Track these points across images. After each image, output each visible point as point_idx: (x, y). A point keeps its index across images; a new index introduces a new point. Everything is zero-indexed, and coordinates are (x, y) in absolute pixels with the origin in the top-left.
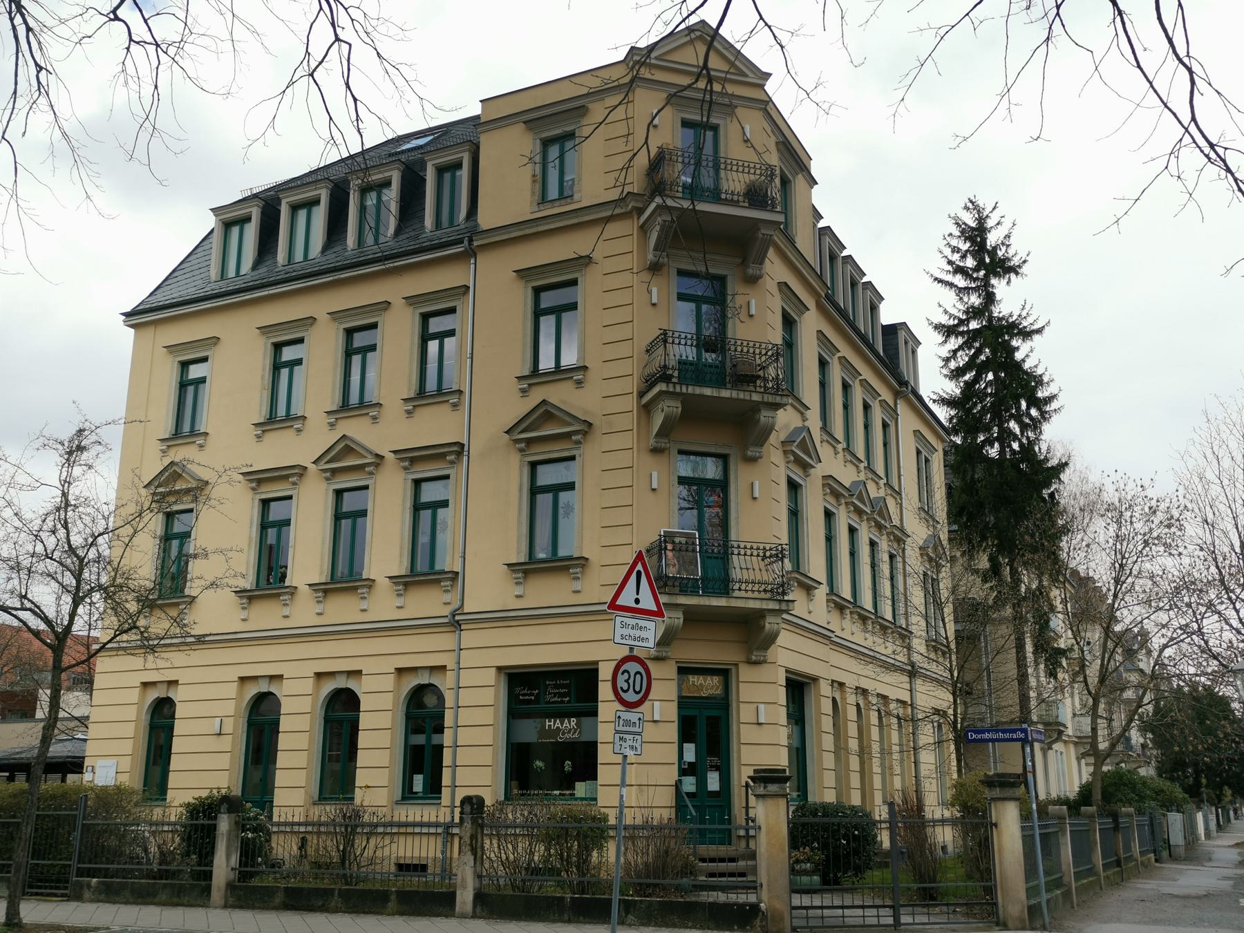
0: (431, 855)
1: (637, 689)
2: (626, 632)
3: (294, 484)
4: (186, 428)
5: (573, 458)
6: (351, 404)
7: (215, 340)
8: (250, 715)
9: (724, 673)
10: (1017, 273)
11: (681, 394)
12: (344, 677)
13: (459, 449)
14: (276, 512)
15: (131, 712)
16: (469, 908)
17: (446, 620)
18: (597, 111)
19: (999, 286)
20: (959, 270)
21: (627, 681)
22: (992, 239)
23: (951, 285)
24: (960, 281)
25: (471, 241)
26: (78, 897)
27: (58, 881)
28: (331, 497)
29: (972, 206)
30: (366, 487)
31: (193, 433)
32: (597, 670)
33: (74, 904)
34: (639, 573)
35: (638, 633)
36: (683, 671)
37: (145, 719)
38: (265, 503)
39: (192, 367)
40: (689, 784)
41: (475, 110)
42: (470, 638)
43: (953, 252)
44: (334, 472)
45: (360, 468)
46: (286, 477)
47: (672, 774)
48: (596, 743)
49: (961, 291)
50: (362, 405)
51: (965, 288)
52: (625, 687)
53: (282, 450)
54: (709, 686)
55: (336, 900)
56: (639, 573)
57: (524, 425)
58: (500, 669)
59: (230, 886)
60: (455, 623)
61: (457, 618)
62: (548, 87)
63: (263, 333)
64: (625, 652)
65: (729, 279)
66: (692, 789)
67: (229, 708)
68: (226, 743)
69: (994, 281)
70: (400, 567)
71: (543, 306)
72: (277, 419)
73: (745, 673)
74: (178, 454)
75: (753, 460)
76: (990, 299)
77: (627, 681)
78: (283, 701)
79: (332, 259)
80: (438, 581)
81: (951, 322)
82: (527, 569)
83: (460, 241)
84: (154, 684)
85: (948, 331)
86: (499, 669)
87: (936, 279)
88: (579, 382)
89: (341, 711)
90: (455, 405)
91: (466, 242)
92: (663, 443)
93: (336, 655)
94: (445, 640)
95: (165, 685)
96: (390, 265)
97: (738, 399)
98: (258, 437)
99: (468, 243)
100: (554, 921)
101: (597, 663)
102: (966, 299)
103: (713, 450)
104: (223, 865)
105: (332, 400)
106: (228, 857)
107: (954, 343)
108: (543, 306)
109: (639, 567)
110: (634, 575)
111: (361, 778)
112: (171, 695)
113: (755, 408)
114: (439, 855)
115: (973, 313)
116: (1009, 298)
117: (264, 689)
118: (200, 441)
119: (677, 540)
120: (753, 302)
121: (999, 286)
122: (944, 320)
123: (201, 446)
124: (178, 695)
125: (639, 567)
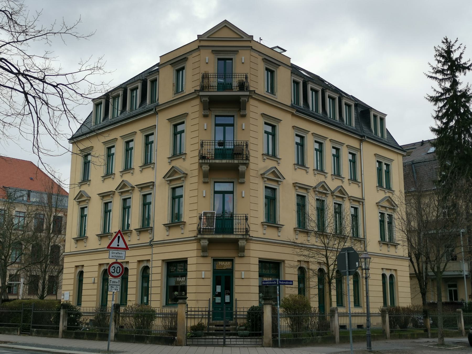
0: (159, 324)
1: (118, 272)
2: (113, 255)
6: (128, 168)
7: (186, 115)
8: (143, 274)
9: (232, 260)
10: (469, 69)
11: (207, 163)
12: (146, 262)
13: (153, 184)
14: (178, 192)
16: (113, 338)
17: (148, 244)
18: (190, 57)
19: (460, 76)
20: (442, 72)
21: (114, 270)
22: (455, 56)
23: (436, 78)
24: (440, 76)
25: (156, 109)
26: (31, 335)
27: (28, 330)
28: (170, 191)
29: (446, 41)
30: (182, 186)
31: (181, 154)
32: (187, 261)
33: (30, 337)
34: (119, 237)
35: (118, 255)
36: (215, 260)
38: (174, 189)
40: (218, 300)
41: (158, 61)
42: (156, 250)
43: (438, 62)
44: (171, 181)
45: (179, 179)
46: (109, 195)
47: (210, 296)
48: (187, 286)
49: (441, 80)
51: (443, 79)
52: (113, 271)
54: (227, 265)
55: (85, 336)
56: (119, 237)
58: (163, 261)
59: (63, 331)
60: (151, 245)
62: (182, 49)
63: (170, 121)
64: (115, 261)
65: (235, 116)
66: (219, 301)
67: (96, 274)
68: (95, 286)
69: (457, 74)
70: (167, 220)
72: (109, 174)
73: (237, 261)
74: (175, 163)
75: (243, 183)
76: (455, 83)
77: (114, 270)
79: (123, 116)
81: (438, 95)
83: (152, 110)
84: (142, 261)
85: (436, 100)
86: (163, 261)
87: (429, 76)
88: (153, 168)
89: (145, 273)
91: (154, 110)
92: (207, 180)
93: (144, 254)
94: (148, 251)
96: (88, 136)
97: (226, 163)
99: (155, 110)
100: (131, 342)
101: (187, 258)
102: (443, 84)
103: (228, 181)
104: (62, 325)
106: (63, 322)
107: (441, 104)
109: (119, 235)
110: (117, 238)
113: (237, 166)
114: (161, 324)
115: (446, 90)
116: (467, 81)
119: (208, 215)
120: (244, 124)
121: (460, 76)
122: (434, 94)
123: (184, 159)
124: (85, 270)
125: (119, 235)
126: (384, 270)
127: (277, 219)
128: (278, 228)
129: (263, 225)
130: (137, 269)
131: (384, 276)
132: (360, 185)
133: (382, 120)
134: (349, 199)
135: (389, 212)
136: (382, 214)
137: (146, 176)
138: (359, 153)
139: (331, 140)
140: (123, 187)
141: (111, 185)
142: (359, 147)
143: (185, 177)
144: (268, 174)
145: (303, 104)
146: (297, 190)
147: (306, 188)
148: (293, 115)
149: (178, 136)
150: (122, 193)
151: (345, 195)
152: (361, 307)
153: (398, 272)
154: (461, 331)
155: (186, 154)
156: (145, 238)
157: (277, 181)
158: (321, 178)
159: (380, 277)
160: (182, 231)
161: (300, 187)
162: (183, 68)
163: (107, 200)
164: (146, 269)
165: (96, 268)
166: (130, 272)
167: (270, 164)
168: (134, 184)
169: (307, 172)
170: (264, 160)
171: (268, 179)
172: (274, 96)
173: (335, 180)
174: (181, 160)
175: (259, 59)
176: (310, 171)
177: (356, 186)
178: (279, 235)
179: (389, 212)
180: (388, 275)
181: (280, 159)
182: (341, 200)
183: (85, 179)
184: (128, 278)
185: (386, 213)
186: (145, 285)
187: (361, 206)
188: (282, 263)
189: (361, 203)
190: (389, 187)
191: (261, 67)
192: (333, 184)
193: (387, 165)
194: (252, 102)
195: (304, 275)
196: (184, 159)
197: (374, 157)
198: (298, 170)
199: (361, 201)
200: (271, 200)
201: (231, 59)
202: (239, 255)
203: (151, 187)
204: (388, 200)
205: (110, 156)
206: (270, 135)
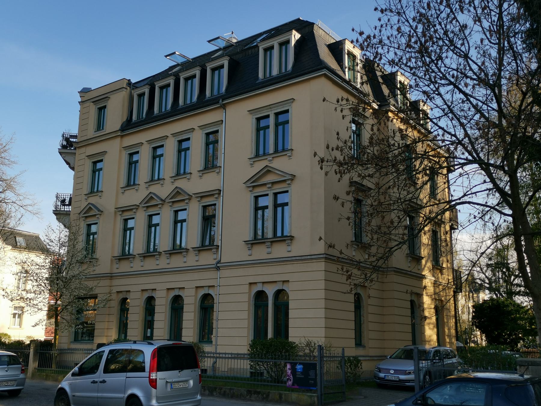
0: (209, 365)
3: (160, 208)
4: (261, 152)
5: (287, 192)
6: (180, 172)
12: (206, 289)
15: (245, 298)
17: (214, 266)
31: (134, 184)
37: (252, 303)
39: (98, 164)
42: (224, 273)
45: (183, 200)
46: (132, 210)
50: (284, 150)
53: (210, 182)
61: (218, 265)
71: (261, 126)
78: (184, 298)
80: (285, 240)
82: (256, 241)
88: (162, 185)
89: (177, 304)
90: (218, 173)
95: (282, 283)
98: (251, 164)
105: (147, 178)
108: (261, 126)
111: (184, 333)
112: (153, 295)
117: (280, 288)
118: (188, 176)
123: (162, 185)
124: (156, 295)
130: (196, 296)
137: (210, 182)
140: (150, 202)
141: (135, 197)
143: (292, 180)
149: (183, 153)
150: (148, 207)
152: (364, 347)
155: (191, 173)
156: (207, 258)
160: (185, 259)
161: (123, 211)
162: (105, 107)
163: (127, 215)
164: (124, 301)
165: (246, 288)
166: (157, 302)
168: (163, 196)
174: (97, 197)
183: (94, 191)
184: (183, 308)
186: (149, 318)
190: (282, 149)
196: (137, 190)
203: (134, 211)
205: (132, 164)
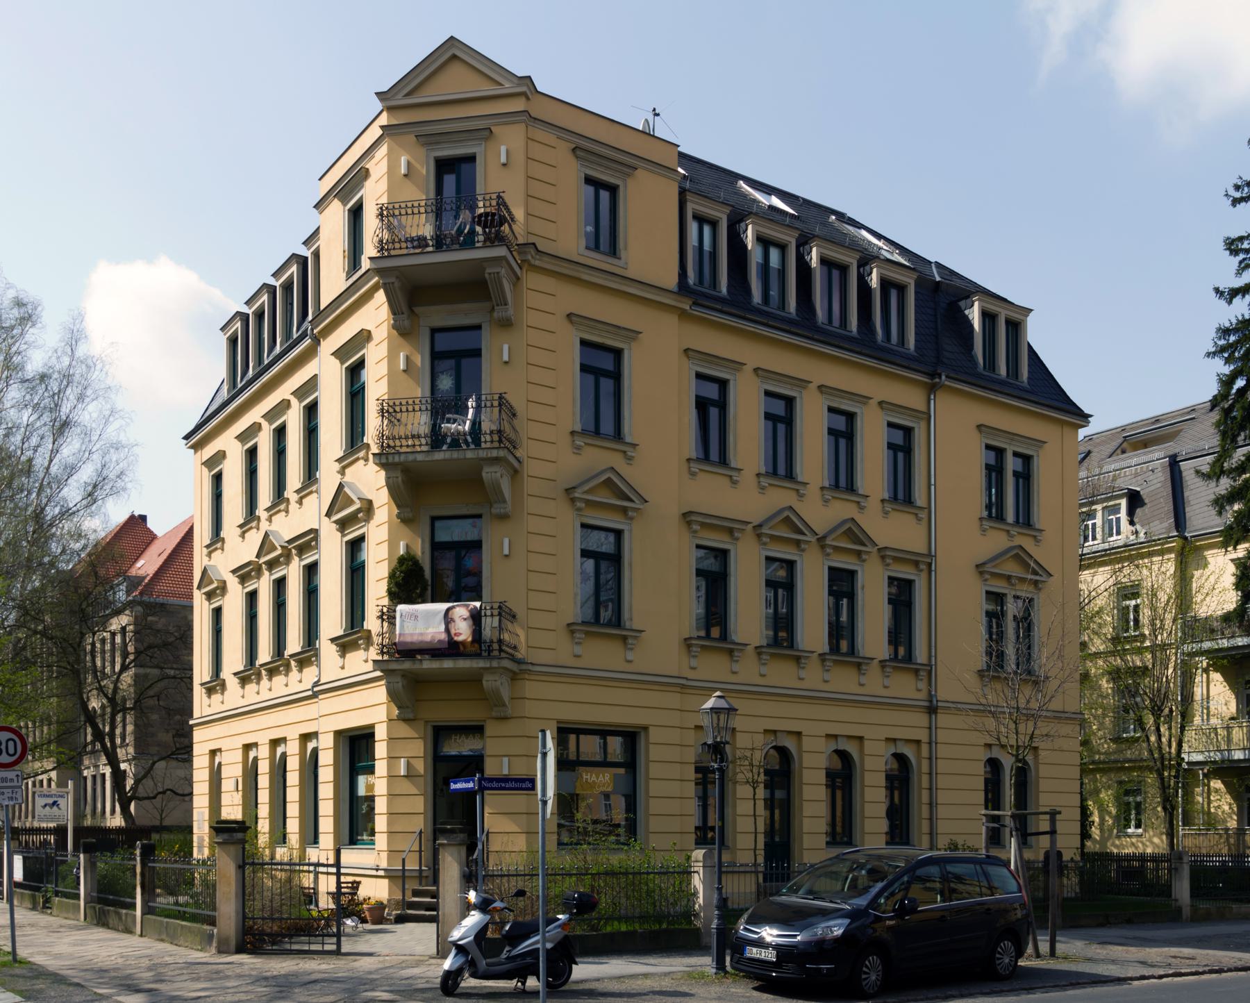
17: (310, 693)
57: (586, 488)
97: (451, 460)
103: (464, 511)
126: (898, 743)
127: (626, 615)
128: (625, 638)
129: (573, 632)
131: (994, 764)
132: (923, 515)
133: (1016, 328)
134: (883, 557)
135: (1025, 591)
136: (997, 598)
138: (923, 424)
139: (821, 388)
142: (923, 408)
144: (772, 523)
145: (859, 326)
146: (695, 532)
147: (730, 528)
148: (683, 314)
151: (864, 545)
153: (866, 743)
154: (1179, 910)
157: (624, 510)
158: (780, 497)
159: (980, 769)
161: (703, 525)
167: (599, 458)
169: (802, 496)
170: (579, 448)
171: (774, 538)
172: (615, 261)
173: (991, 533)
175: (561, 153)
176: (748, 478)
177: (912, 517)
178: (629, 658)
179: (1025, 591)
180: (1008, 762)
181: (634, 445)
182: (726, 538)
185: (1010, 593)
187: (924, 575)
188: (643, 734)
189: (923, 567)
190: (1025, 520)
191: (570, 174)
192: (821, 513)
193: (1027, 459)
194: (532, 280)
195: (1026, 776)
197: (975, 434)
198: (894, 515)
199: (925, 562)
200: (607, 564)
201: (471, 159)
202: (494, 714)
204: (1017, 556)
206: (781, 422)
